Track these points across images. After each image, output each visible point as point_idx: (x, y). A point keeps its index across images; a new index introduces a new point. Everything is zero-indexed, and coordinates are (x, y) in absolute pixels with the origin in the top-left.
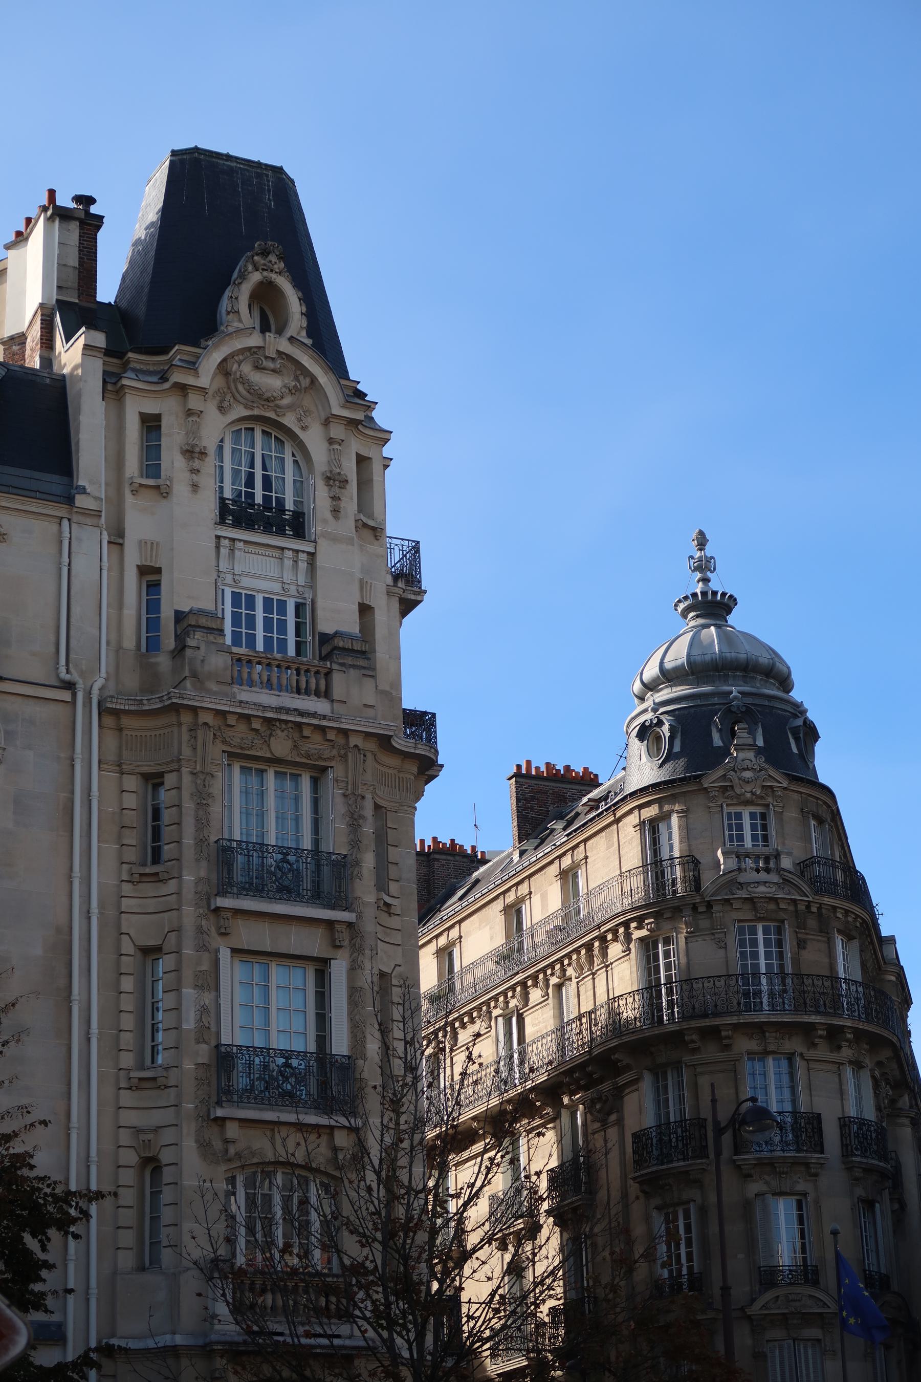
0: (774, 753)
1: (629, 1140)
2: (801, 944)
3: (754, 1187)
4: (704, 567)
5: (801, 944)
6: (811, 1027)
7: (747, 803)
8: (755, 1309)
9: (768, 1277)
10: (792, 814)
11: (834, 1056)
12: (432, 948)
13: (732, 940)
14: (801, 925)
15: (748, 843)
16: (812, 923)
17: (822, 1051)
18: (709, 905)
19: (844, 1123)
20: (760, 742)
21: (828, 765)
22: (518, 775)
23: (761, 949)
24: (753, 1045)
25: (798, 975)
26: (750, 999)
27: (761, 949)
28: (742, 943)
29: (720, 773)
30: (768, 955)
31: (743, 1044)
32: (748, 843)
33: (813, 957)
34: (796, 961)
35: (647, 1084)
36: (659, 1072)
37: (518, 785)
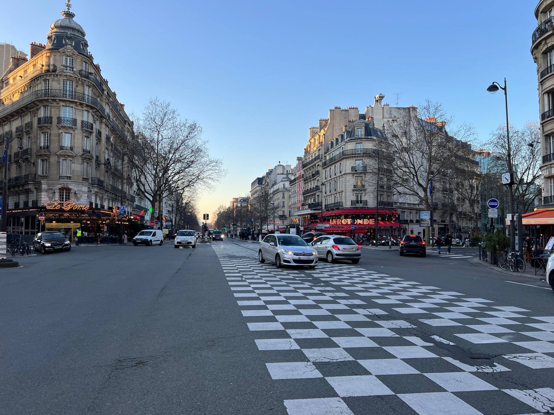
0: (76, 47)
1: (498, 87)
2: (77, 86)
3: (60, 131)
4: (69, 6)
5: (77, 86)
6: (76, 102)
7: (68, 56)
8: (58, 153)
9: (62, 148)
10: (79, 60)
11: (82, 109)
12: (12, 78)
13: (62, 83)
14: (77, 82)
15: (68, 64)
16: (80, 82)
17: (79, 107)
18: (57, 75)
19: (82, 122)
20: (73, 44)
21: (90, 50)
22: (32, 44)
23: (68, 86)
24: (64, 104)
25: (75, 92)
26: (64, 95)
27: (68, 86)
28: (64, 84)
29: (63, 49)
30: (69, 87)
31: (62, 104)
32: (68, 64)
33: (79, 89)
34: (75, 89)
35: (42, 108)
36: (45, 106)
37: (32, 47)
